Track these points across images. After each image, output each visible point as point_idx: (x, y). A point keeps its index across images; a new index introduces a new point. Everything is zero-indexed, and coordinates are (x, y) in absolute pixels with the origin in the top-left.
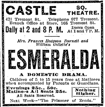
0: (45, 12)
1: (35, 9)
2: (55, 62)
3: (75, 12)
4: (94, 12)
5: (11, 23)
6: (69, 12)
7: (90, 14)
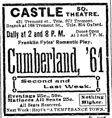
0: (51, 14)
3: (74, 13)
4: (94, 14)
5: (8, 26)
6: (68, 13)
7: (89, 16)
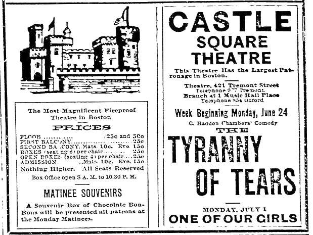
1: (238, 18)
2: (200, 153)
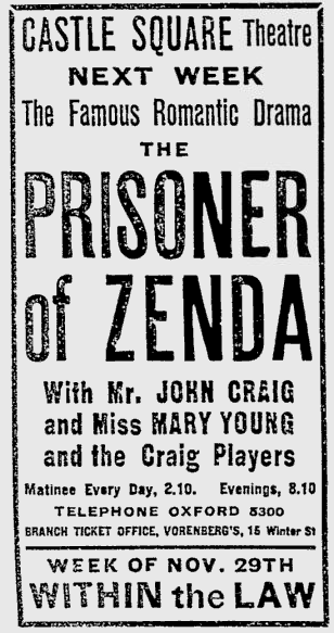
4: (178, 150)
6: (147, 145)
